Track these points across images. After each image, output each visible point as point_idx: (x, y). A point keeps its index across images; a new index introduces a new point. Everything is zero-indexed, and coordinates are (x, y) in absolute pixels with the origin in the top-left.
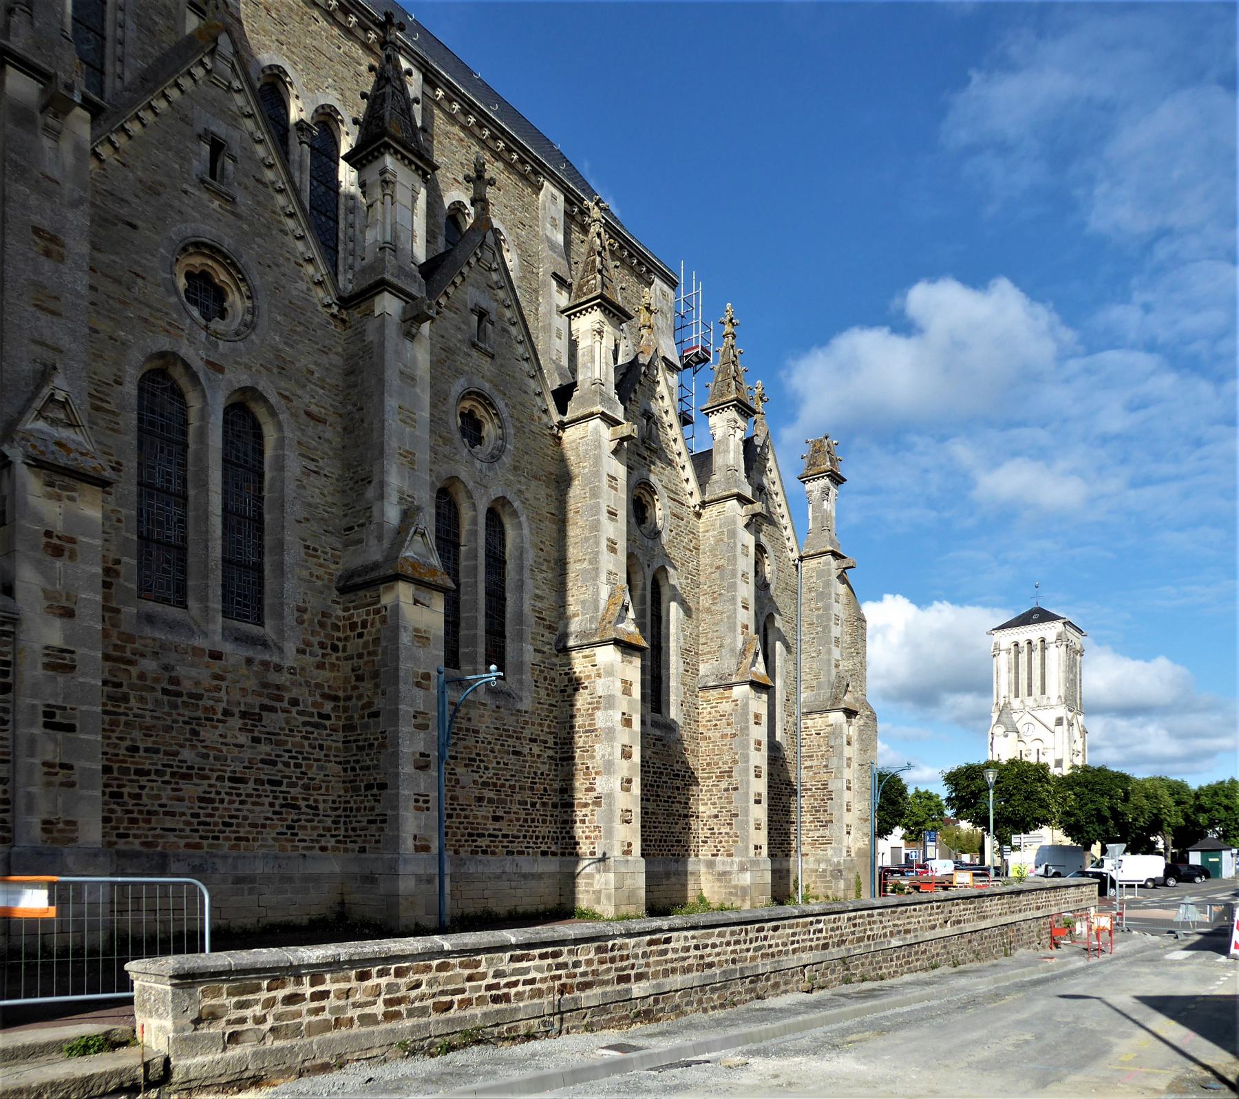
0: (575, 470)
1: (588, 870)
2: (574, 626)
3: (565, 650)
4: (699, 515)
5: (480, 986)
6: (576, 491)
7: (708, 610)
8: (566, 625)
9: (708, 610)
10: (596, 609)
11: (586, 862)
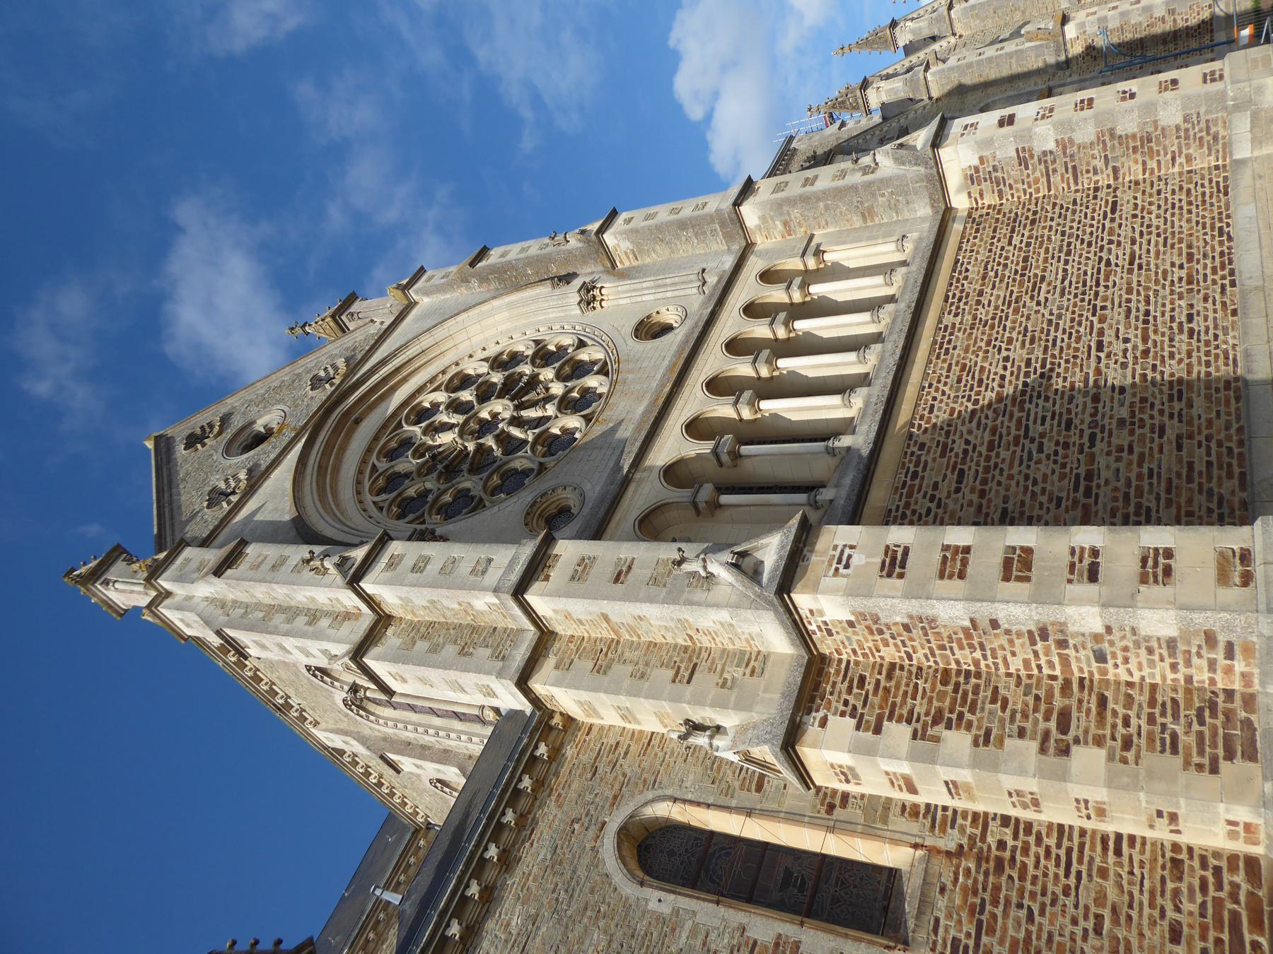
0: (956, 83)
1: (1222, 7)
2: (1051, 60)
3: (1068, 63)
4: (961, 36)
5: (1216, 747)
6: (968, 80)
7: (1023, 12)
8: (1051, 66)
9: (1023, 12)
10: (1041, 46)
11: (1217, 10)
